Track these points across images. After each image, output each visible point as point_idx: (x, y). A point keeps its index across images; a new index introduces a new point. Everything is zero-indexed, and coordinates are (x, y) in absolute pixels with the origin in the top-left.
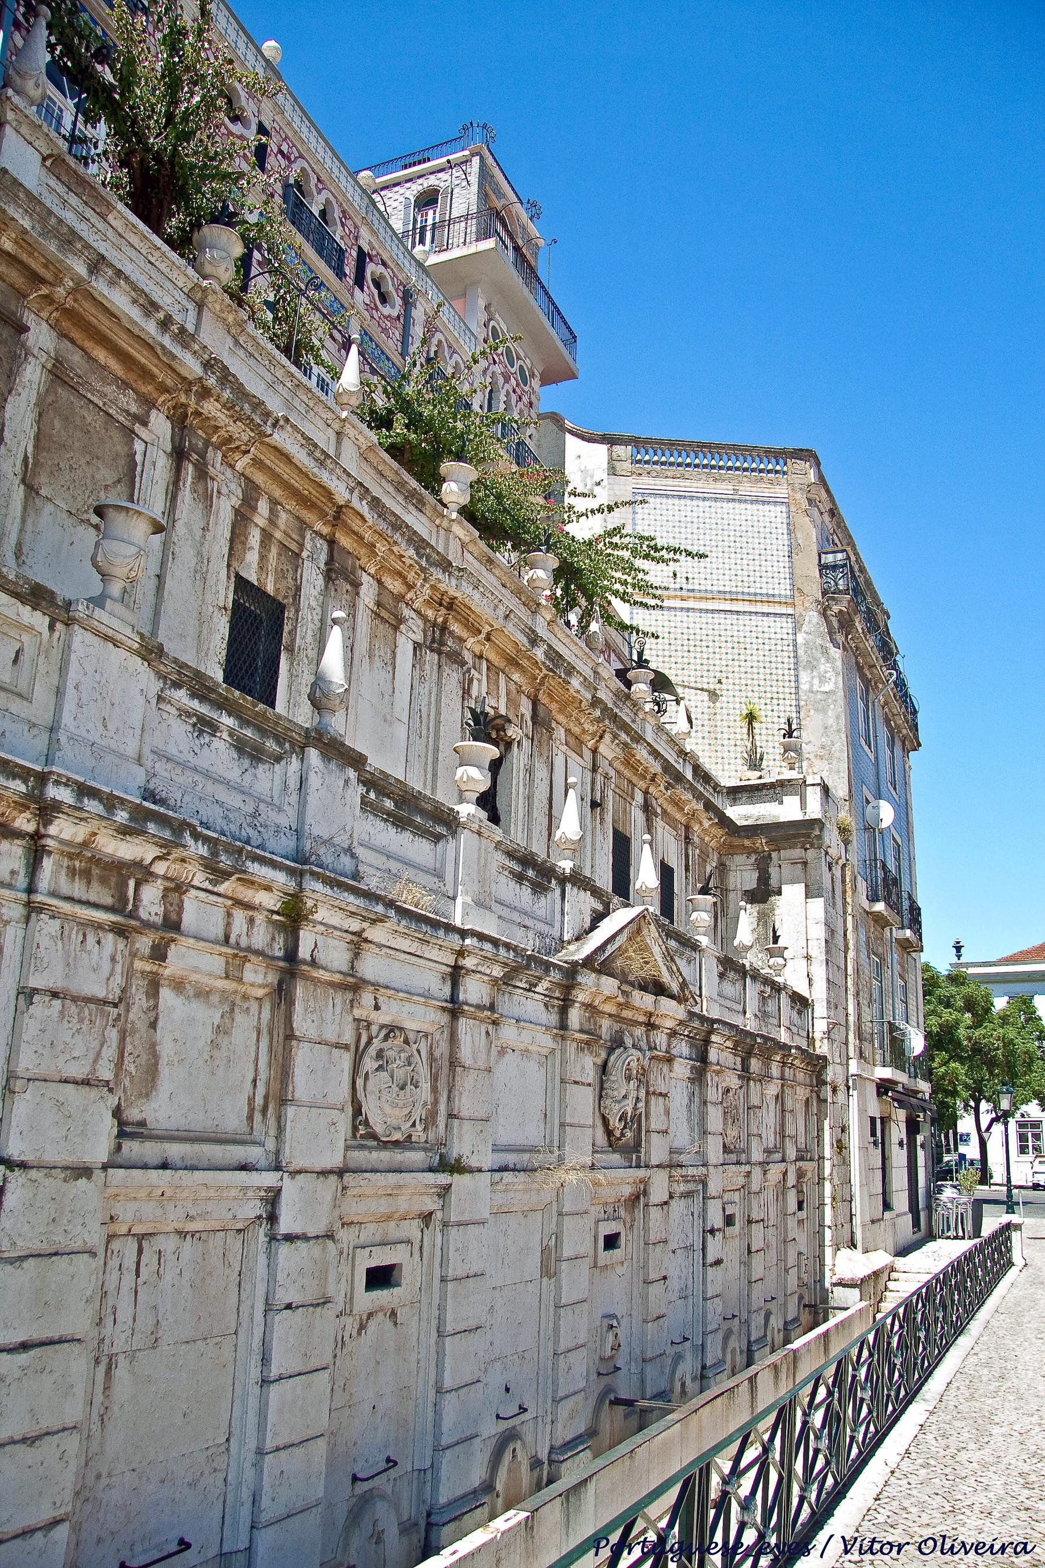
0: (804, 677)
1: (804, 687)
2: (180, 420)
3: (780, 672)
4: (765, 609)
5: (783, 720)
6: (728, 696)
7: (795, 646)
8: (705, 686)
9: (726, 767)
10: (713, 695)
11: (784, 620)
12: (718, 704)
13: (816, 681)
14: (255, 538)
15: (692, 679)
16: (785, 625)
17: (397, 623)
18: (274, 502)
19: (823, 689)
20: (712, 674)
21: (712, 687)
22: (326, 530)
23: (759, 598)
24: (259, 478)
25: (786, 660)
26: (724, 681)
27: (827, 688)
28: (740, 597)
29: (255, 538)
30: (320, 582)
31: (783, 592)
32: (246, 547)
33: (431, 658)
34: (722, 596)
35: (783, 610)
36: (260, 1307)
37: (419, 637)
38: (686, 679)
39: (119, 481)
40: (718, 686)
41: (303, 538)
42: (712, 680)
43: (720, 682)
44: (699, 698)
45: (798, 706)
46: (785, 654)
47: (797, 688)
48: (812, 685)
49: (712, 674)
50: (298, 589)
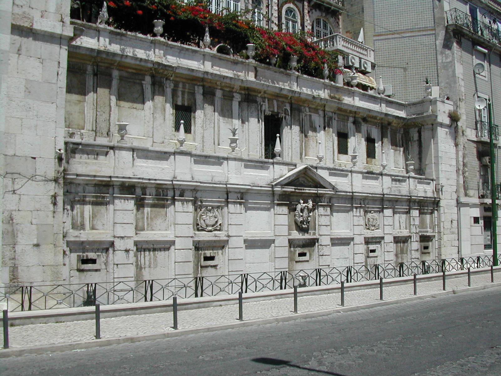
0: (439, 57)
1: (440, 61)
2: (153, 76)
3: (430, 57)
4: (424, 33)
5: (425, 78)
6: (410, 69)
7: (436, 46)
8: (402, 66)
9: (411, 95)
10: (405, 69)
11: (431, 36)
13: (444, 58)
14: (180, 94)
16: (431, 38)
17: (231, 98)
18: (183, 83)
19: (447, 61)
21: (404, 66)
22: (201, 84)
23: (421, 29)
24: (178, 79)
25: (432, 52)
26: (409, 63)
27: (449, 60)
28: (414, 30)
29: (180, 94)
30: (202, 97)
31: (431, 25)
32: (178, 97)
33: (245, 104)
34: (407, 31)
35: (431, 32)
36: (383, 225)
37: (240, 100)
38: (395, 65)
39: (140, 96)
40: (407, 65)
41: (194, 88)
42: (404, 64)
43: (407, 64)
45: (437, 69)
46: (432, 49)
47: (437, 62)
48: (442, 60)
49: (404, 61)
50: (195, 101)
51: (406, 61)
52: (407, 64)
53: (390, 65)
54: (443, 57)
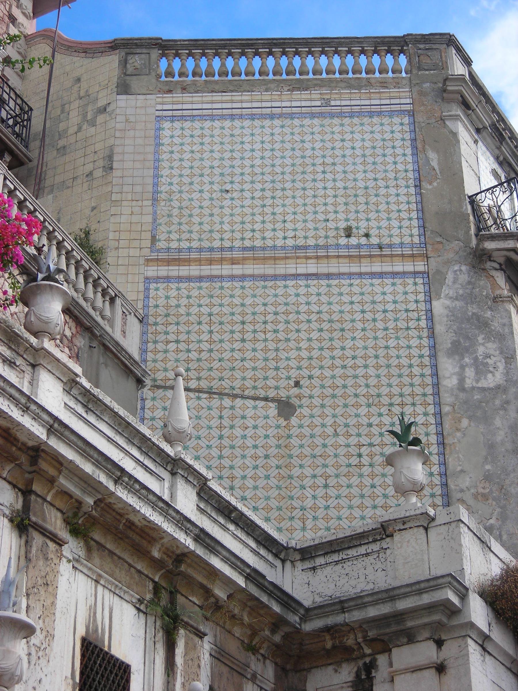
12: (294, 421)
13: (470, 373)
15: (249, 383)
20: (283, 374)
43: (297, 384)
44: (261, 412)
48: (462, 380)
51: (294, 373)
52: (297, 384)
53: (216, 384)
54: (462, 368)
